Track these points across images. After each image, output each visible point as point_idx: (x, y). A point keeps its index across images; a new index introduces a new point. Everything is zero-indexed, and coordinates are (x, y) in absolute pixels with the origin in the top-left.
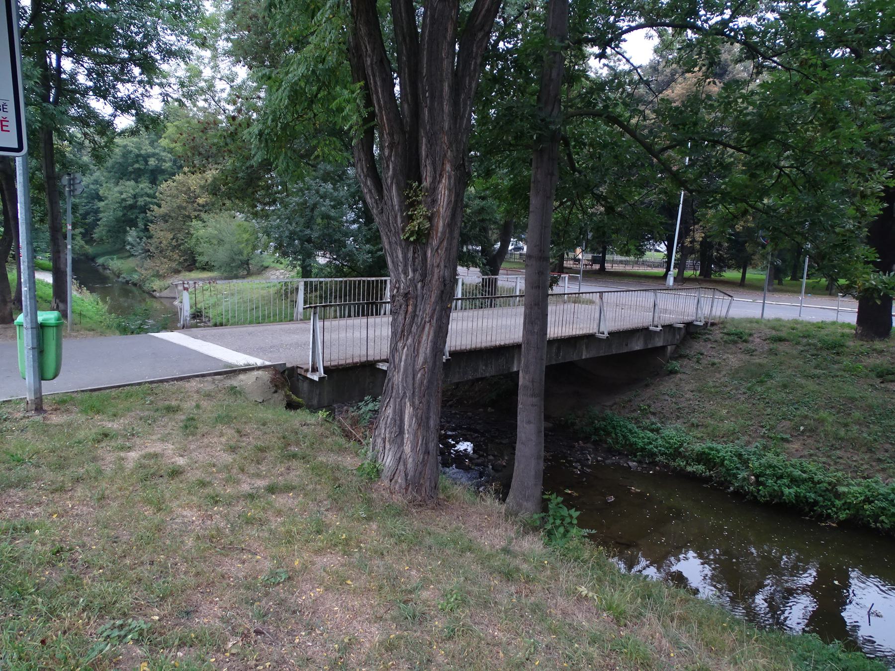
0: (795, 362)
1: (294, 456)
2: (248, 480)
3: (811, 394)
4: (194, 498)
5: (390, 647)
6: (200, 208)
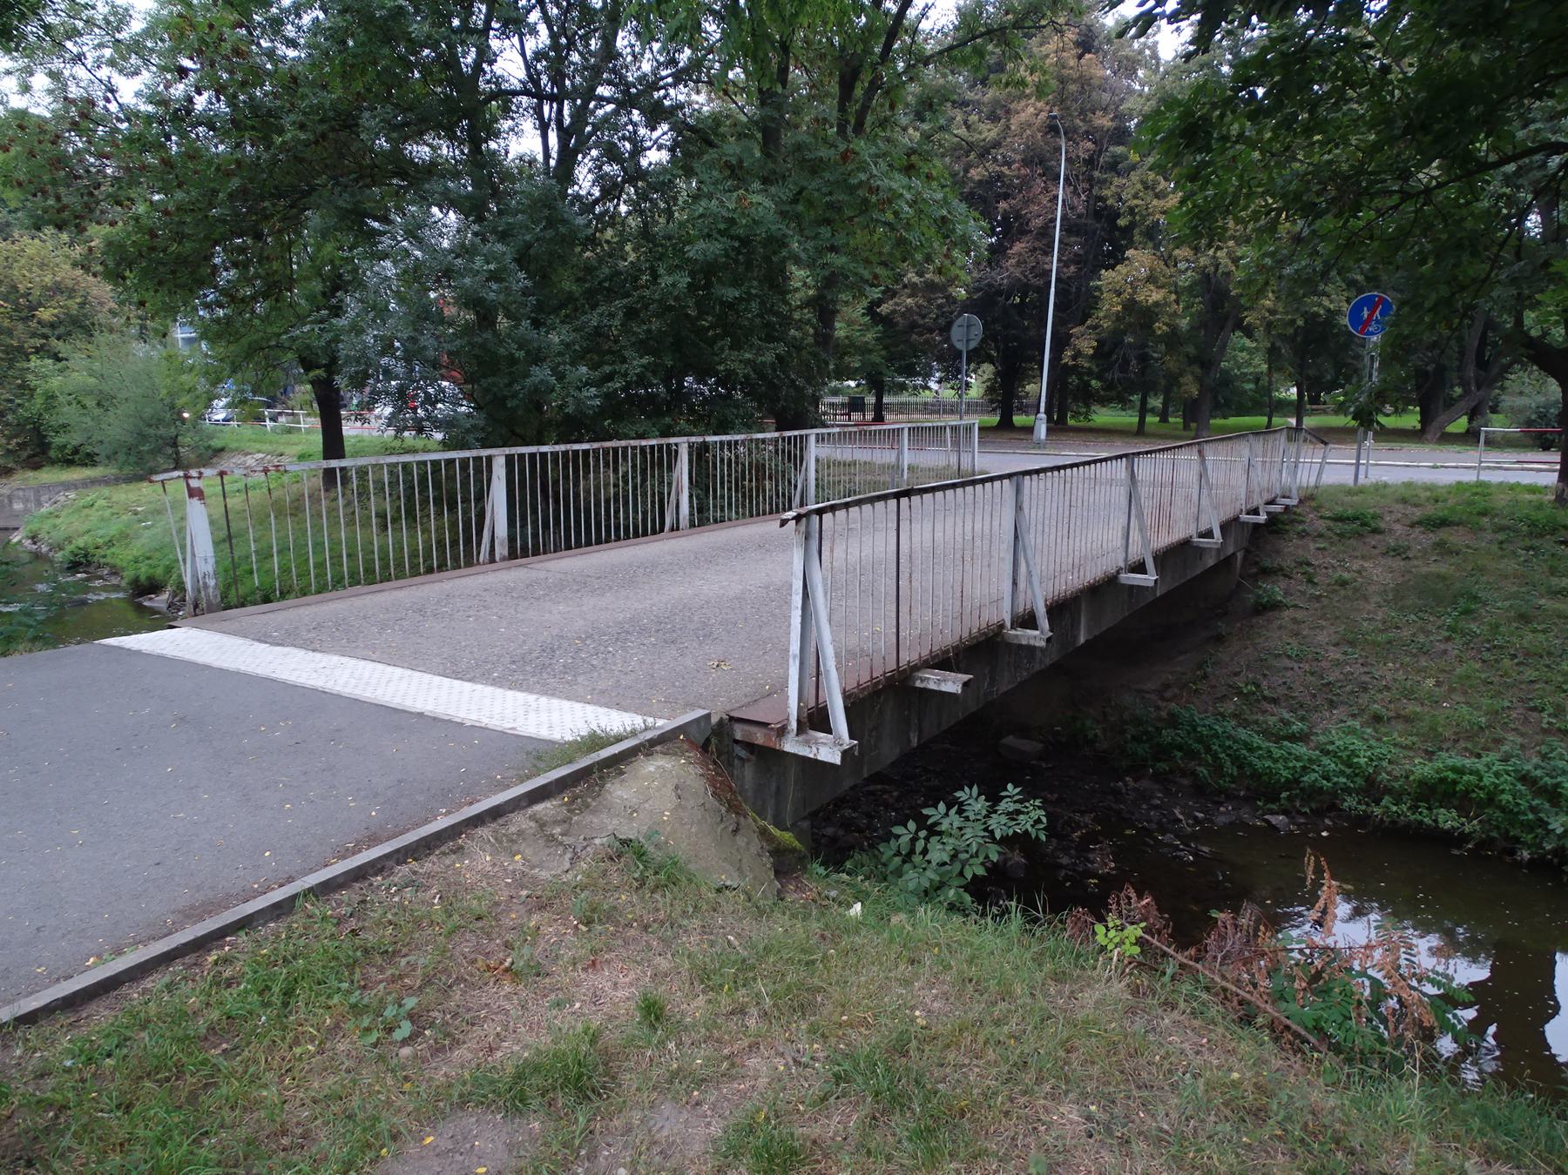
6: (45, 330)
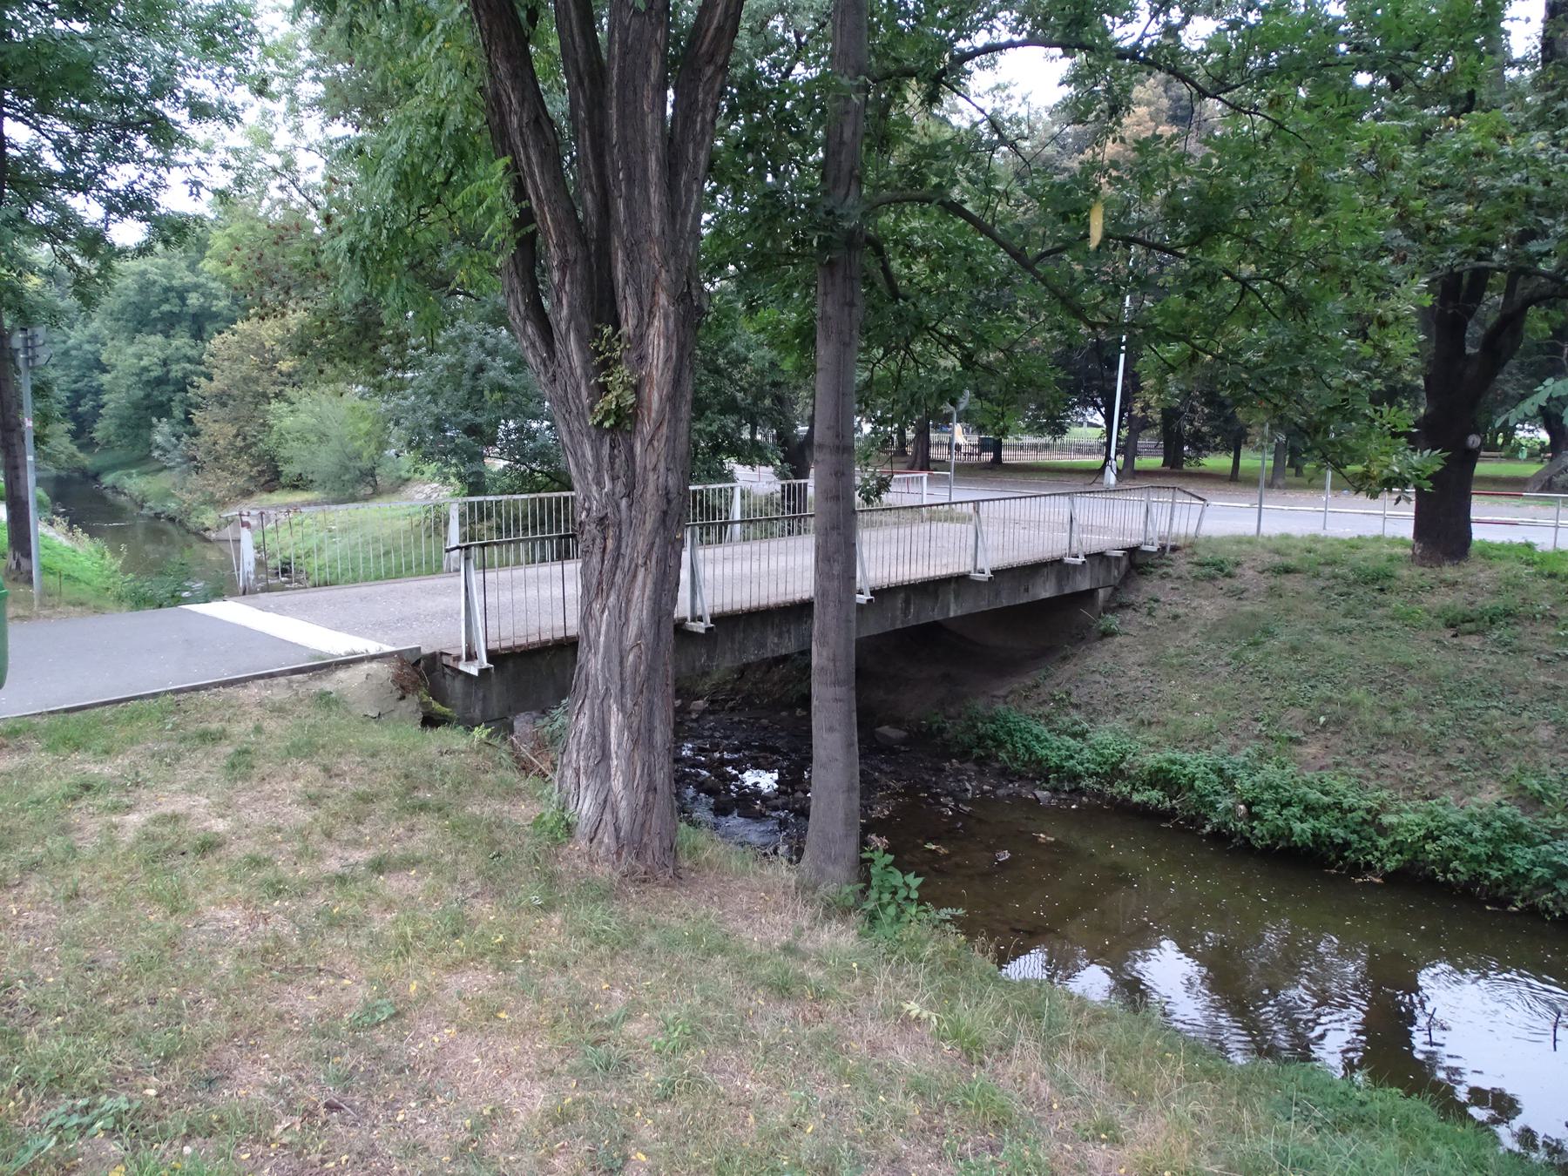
0: (1311, 608)
1: (423, 807)
2: (338, 851)
3: (1337, 661)
4: (239, 888)
5: (561, 1118)
6: (284, 379)
